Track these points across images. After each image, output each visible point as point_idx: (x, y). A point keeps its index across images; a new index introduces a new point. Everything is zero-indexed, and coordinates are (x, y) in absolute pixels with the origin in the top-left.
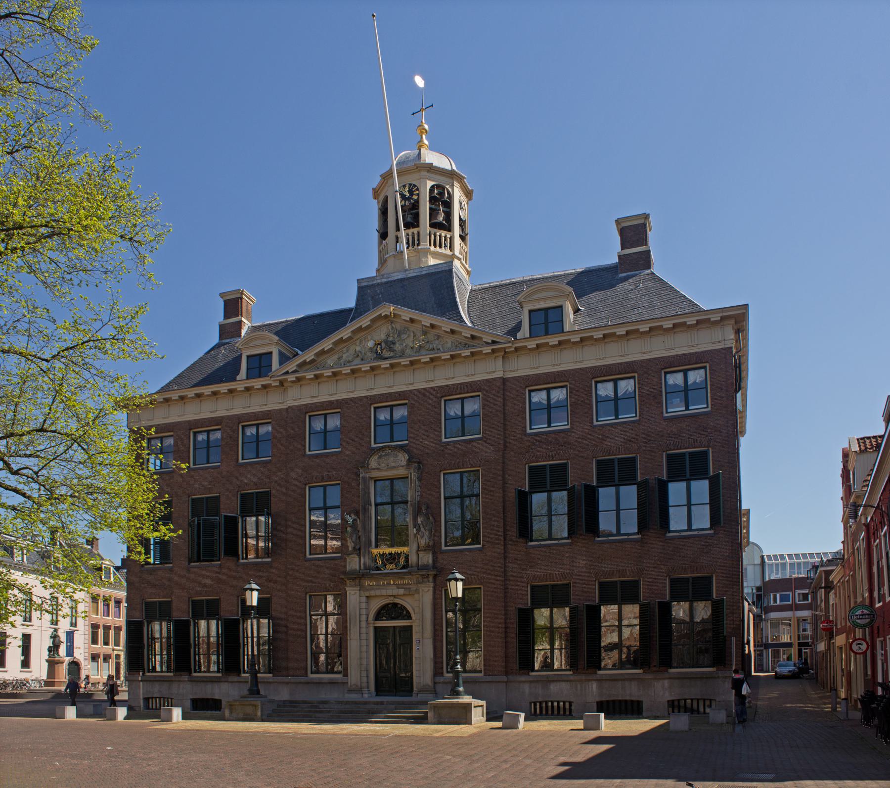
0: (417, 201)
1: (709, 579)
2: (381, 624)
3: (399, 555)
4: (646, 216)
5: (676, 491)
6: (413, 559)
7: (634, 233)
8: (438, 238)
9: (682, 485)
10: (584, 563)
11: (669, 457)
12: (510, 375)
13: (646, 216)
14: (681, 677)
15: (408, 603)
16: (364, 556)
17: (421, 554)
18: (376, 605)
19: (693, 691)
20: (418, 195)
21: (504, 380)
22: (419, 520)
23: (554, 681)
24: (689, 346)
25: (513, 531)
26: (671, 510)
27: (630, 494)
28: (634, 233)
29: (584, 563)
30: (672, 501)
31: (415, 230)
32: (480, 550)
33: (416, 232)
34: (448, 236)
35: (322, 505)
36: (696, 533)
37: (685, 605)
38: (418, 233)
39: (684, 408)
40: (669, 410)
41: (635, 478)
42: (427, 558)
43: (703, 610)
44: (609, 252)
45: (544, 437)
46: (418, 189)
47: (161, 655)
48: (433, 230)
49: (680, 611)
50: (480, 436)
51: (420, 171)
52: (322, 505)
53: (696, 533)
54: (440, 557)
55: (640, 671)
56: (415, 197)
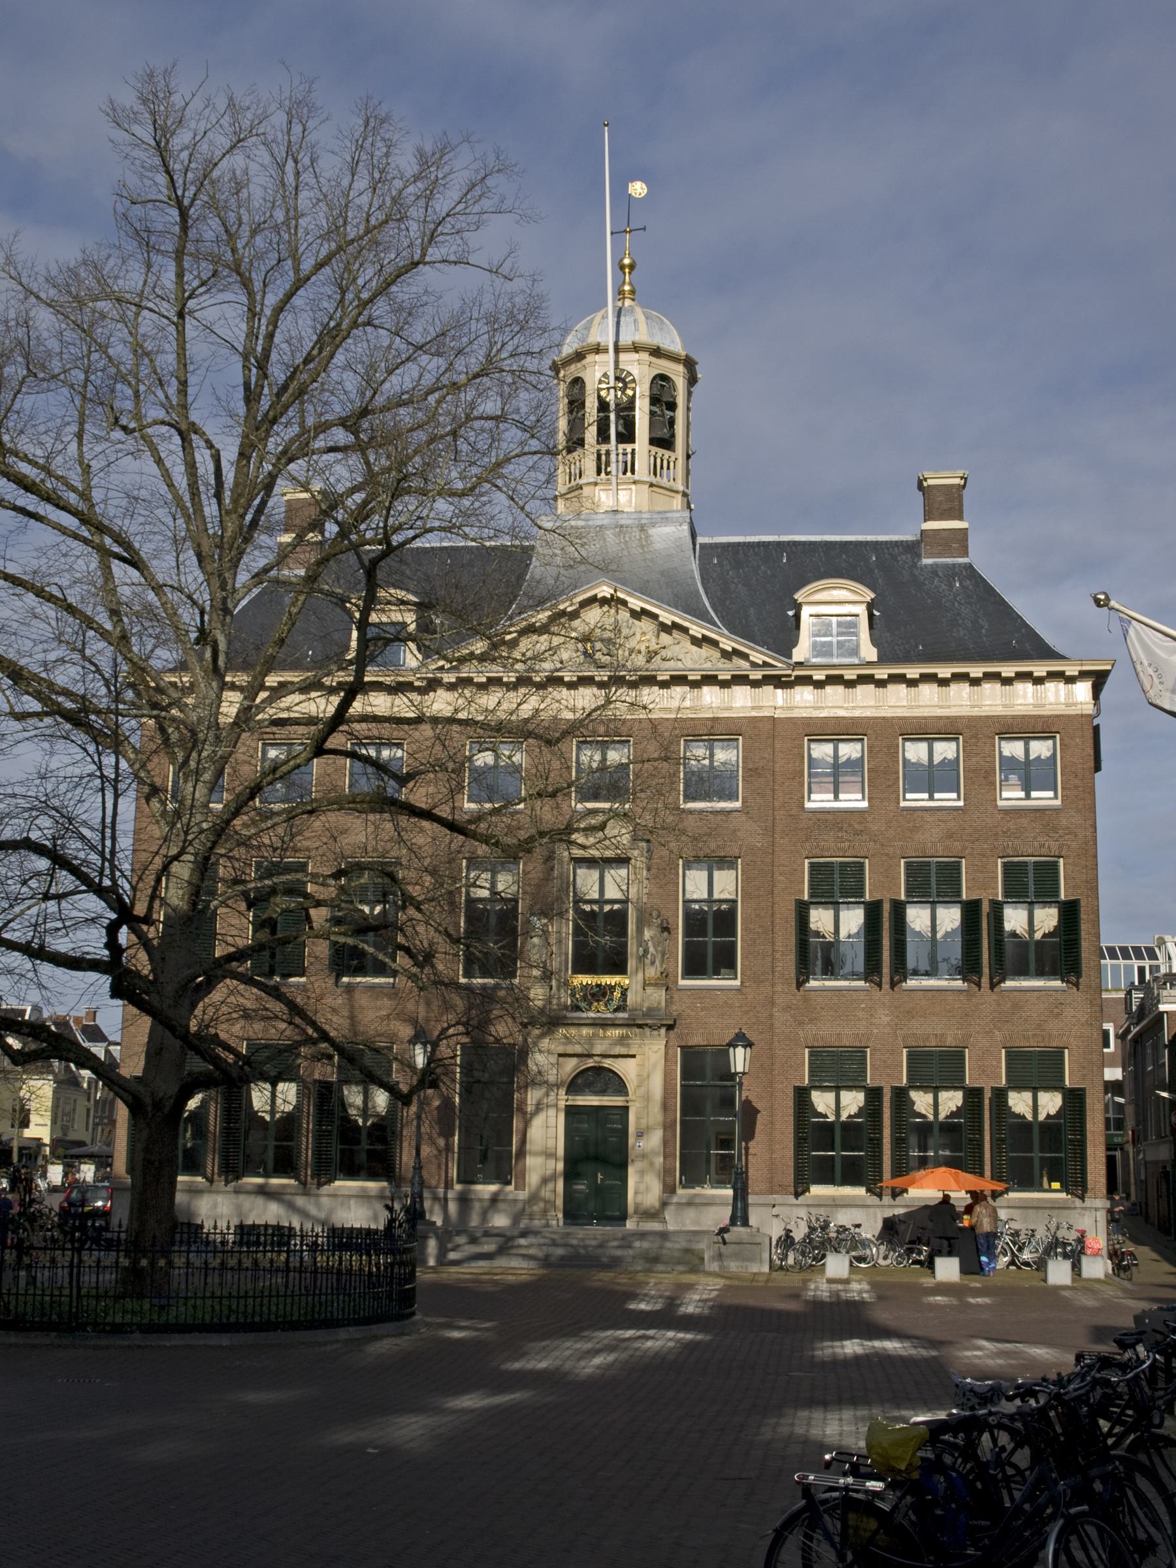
0: (632, 400)
1: (1058, 1055)
3: (612, 988)
8: (659, 461)
10: (888, 1019)
15: (627, 1069)
17: (649, 990)
21: (772, 719)
22: (647, 934)
23: (843, 1206)
29: (888, 1019)
31: (629, 448)
33: (629, 450)
37: (1027, 1096)
38: (633, 450)
42: (658, 996)
43: (1051, 1103)
45: (830, 817)
47: (308, 1129)
48: (654, 449)
49: (917, 918)
54: (676, 997)
55: (1057, 983)
56: (630, 392)
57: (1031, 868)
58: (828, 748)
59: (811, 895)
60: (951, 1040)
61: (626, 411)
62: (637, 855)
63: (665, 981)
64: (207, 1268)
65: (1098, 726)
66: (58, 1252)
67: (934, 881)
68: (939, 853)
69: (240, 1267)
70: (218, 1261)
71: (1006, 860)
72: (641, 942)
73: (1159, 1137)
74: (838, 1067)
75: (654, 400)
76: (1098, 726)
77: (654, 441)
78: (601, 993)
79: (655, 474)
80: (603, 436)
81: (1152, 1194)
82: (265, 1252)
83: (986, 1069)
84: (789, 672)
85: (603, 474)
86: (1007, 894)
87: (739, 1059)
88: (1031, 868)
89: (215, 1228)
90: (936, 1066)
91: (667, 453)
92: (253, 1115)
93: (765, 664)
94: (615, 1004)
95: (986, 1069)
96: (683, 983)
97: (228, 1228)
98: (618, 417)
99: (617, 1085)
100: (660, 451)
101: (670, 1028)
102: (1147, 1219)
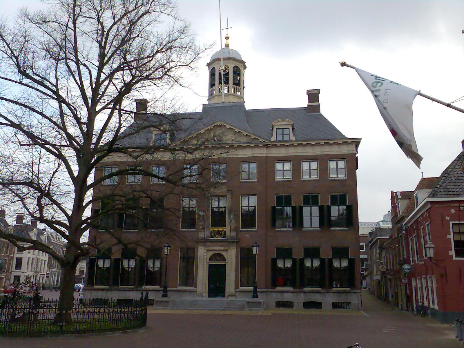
0: (228, 73)
2: (212, 263)
3: (221, 231)
4: (319, 90)
5: (306, 210)
6: (228, 234)
7: (313, 96)
8: (235, 89)
9: (309, 208)
11: (331, 196)
12: (268, 155)
13: (319, 90)
14: (338, 292)
16: (207, 231)
18: (211, 254)
19: (342, 299)
20: (229, 70)
21: (266, 157)
22: (231, 216)
24: (286, 153)
25: (270, 224)
26: (304, 218)
27: (315, 210)
28: (313, 96)
30: (305, 215)
32: (255, 231)
34: (239, 88)
35: (250, 205)
36: (314, 229)
39: (282, 178)
40: (277, 178)
41: (346, 203)
42: (234, 234)
44: (303, 102)
46: (228, 68)
48: (234, 86)
50: (256, 180)
51: (215, 62)
52: (250, 205)
53: (314, 229)
56: (227, 71)
57: (284, 197)
58: (217, 167)
59: (277, 205)
60: (316, 245)
61: (227, 75)
62: (229, 195)
63: (236, 229)
64: (94, 313)
65: (357, 157)
66: (96, 309)
67: (311, 200)
68: (338, 193)
69: (109, 313)
70: (98, 310)
71: (277, 195)
72: (229, 218)
73: (377, 273)
74: (284, 252)
75: (234, 72)
76: (357, 157)
77: (234, 84)
78: (219, 233)
79: (234, 93)
80: (220, 83)
81: (375, 288)
82: (47, 308)
83: (326, 253)
84: (270, 144)
85: (220, 93)
86: (304, 204)
87: (255, 250)
88: (338, 196)
89: (112, 300)
90: (312, 252)
91: (238, 87)
92: (123, 268)
93: (263, 141)
94: (223, 235)
95: (326, 253)
96: (241, 229)
97: (115, 301)
98: (224, 77)
99: (224, 259)
100: (236, 87)
101: (237, 242)
102: (374, 295)
